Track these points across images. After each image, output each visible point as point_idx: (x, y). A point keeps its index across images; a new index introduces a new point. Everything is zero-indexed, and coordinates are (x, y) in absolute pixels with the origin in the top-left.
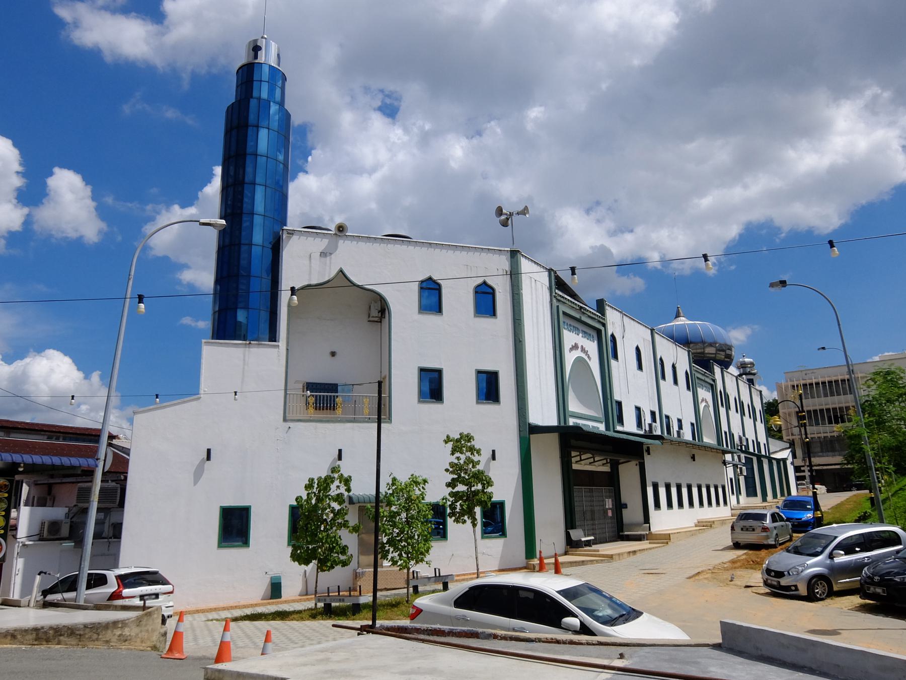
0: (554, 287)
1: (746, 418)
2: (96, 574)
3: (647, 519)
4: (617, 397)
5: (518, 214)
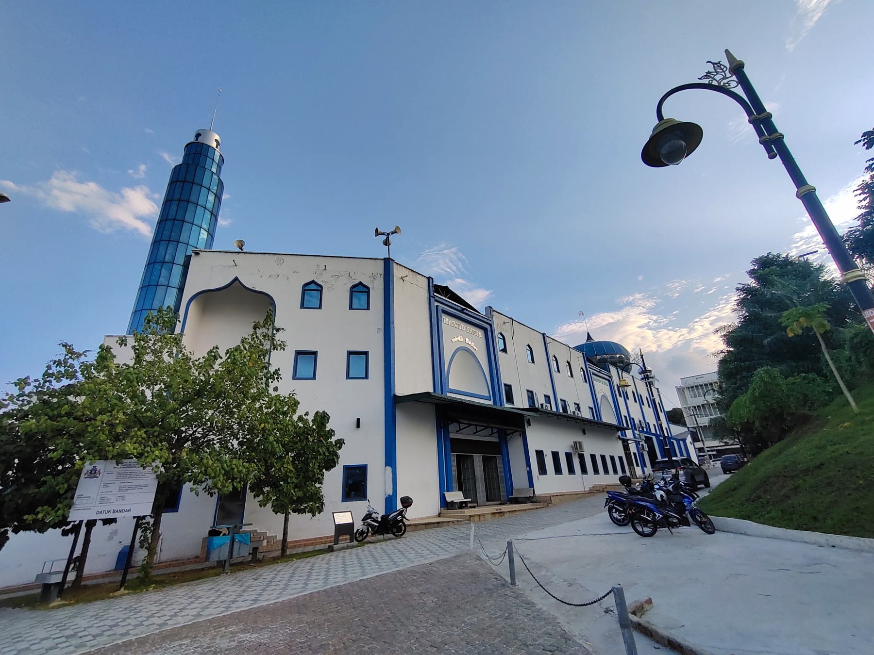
0: (431, 289)
1: (645, 408)
2: (342, 595)
3: (531, 484)
4: (504, 380)
5: (393, 233)
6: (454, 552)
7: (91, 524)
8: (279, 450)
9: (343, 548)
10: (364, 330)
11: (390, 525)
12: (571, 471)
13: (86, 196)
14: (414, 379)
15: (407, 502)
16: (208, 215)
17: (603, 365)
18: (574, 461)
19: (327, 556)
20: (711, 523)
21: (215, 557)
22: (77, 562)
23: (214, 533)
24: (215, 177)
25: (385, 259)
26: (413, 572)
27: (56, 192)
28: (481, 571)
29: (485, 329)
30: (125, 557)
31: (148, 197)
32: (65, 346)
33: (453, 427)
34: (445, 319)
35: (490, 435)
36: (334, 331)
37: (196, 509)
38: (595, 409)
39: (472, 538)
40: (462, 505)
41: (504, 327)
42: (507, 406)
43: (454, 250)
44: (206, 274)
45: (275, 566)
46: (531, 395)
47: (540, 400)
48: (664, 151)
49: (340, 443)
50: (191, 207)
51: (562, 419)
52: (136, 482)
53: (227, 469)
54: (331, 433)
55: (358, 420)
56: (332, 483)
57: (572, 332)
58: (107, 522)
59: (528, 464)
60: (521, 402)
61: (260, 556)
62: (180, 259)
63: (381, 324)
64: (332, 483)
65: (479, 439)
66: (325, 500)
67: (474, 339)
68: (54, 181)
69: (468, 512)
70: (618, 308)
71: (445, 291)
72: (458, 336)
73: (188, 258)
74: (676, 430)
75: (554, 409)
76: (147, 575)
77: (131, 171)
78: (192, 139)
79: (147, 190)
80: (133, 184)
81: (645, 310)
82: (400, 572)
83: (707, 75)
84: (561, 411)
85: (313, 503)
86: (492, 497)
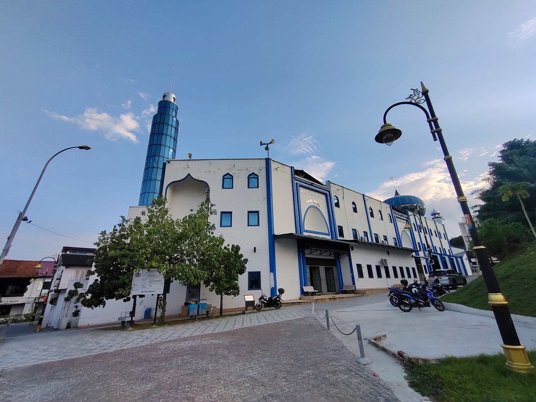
0: (293, 173)
3: (354, 283)
6: (304, 316)
7: (135, 297)
8: (217, 264)
9: (250, 313)
10: (256, 200)
11: (273, 302)
12: (379, 276)
13: (102, 121)
14: (284, 226)
15: (282, 291)
16: (172, 139)
17: (404, 211)
18: (381, 270)
19: (242, 316)
20: (443, 306)
21: (191, 313)
22: (132, 314)
23: (186, 304)
24: (174, 118)
25: (266, 159)
26: (283, 323)
27: (87, 120)
28: (315, 324)
29: (326, 195)
30: (148, 312)
31: (133, 118)
32: (122, 217)
33: (307, 251)
34: (302, 191)
35: (329, 256)
36: (239, 200)
37: (178, 294)
38: (398, 239)
39: (313, 310)
40: (313, 294)
41: (338, 192)
42: (339, 238)
43: (310, 137)
44: (174, 173)
45: (218, 319)
46: (355, 231)
47: (361, 234)
48: (385, 137)
49: (246, 261)
50: (164, 136)
51: (376, 246)
52: (155, 279)
53: (195, 274)
54: (241, 256)
55: (255, 248)
56: (243, 280)
57: (380, 195)
58: (141, 296)
59: (352, 272)
60: (348, 236)
61: (210, 315)
62: (161, 165)
63: (265, 196)
64: (243, 280)
65: (323, 259)
66: (240, 289)
67: (319, 200)
68: (86, 114)
69: (316, 297)
70: (423, 169)
71: (301, 173)
72: (309, 199)
73: (165, 164)
74: (456, 251)
75: (370, 241)
76: (163, 321)
77: (123, 105)
78: (161, 99)
79: (132, 115)
80: (125, 112)
81: (442, 170)
82: (276, 323)
83: (410, 97)
84: (375, 242)
85: (235, 290)
86: (330, 289)
